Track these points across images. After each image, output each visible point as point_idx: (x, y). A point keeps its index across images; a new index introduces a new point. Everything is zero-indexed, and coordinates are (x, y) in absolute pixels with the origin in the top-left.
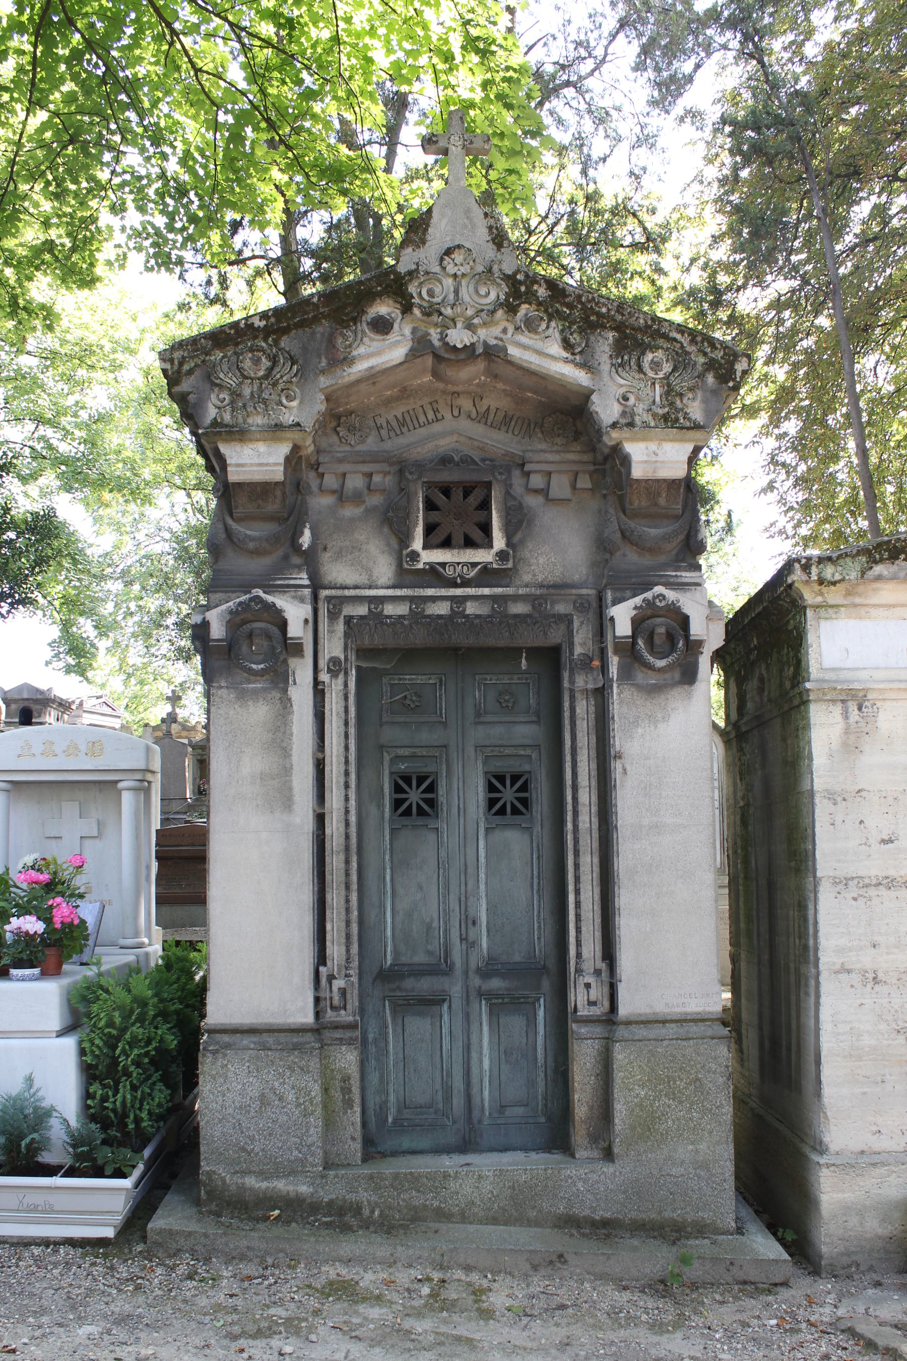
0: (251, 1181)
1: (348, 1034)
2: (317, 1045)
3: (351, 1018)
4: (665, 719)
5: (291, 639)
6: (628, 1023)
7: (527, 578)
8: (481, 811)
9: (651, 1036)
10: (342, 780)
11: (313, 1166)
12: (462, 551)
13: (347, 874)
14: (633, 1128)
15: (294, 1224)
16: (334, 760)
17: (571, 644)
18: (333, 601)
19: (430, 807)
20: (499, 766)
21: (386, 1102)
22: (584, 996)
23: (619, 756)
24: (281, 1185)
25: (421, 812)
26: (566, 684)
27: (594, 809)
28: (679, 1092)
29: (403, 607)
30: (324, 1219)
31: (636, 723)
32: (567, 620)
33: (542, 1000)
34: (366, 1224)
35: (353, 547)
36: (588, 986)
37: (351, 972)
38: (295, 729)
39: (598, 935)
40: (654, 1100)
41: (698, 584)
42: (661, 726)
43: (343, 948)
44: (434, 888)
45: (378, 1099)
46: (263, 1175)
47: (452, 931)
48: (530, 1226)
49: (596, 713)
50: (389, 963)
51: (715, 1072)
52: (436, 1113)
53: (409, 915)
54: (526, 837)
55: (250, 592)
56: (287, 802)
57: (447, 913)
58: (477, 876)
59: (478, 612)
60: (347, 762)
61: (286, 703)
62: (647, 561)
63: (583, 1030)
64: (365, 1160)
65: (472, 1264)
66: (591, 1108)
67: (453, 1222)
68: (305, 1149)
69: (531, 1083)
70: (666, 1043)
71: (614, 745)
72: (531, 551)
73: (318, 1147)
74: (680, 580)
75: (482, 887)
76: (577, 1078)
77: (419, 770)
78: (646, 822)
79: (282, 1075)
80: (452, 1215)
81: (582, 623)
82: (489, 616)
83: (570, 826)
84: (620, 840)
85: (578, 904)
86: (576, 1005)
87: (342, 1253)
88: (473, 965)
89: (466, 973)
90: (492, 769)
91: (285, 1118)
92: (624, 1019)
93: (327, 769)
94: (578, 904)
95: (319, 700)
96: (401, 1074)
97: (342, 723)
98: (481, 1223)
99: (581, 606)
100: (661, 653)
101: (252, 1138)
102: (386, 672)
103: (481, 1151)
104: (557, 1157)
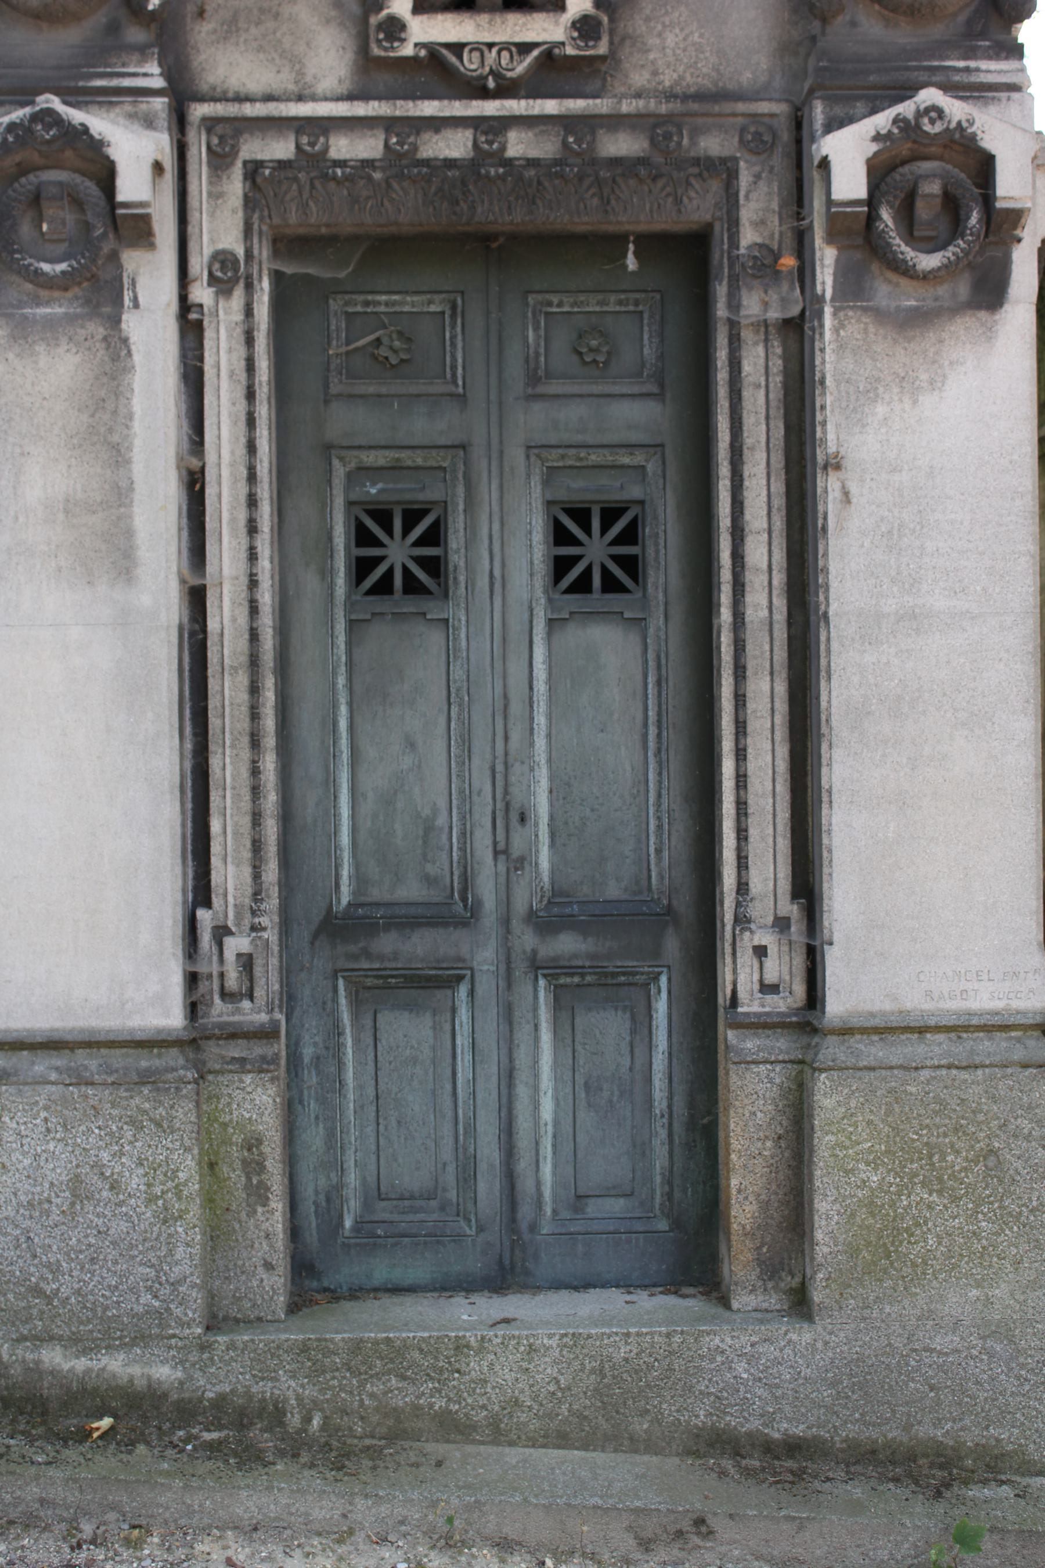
0: (53, 1357)
1: (258, 1049)
2: (190, 1075)
3: (263, 1017)
4: (935, 384)
5: (125, 205)
6: (846, 1031)
7: (639, 79)
8: (539, 583)
9: (894, 1061)
10: (242, 516)
11: (182, 1324)
12: (498, 18)
13: (255, 715)
14: (853, 1252)
15: (141, 1449)
16: (225, 472)
17: (734, 223)
18: (219, 129)
19: (429, 577)
20: (577, 488)
21: (340, 1187)
22: (753, 972)
23: (835, 464)
24: (118, 1366)
25: (412, 586)
26: (721, 311)
27: (779, 579)
28: (953, 1177)
29: (372, 142)
30: (207, 1436)
31: (871, 393)
32: (724, 170)
33: (664, 980)
34: (294, 1447)
35: (262, 11)
36: (761, 952)
37: (265, 921)
38: (138, 405)
39: (784, 844)
40: (899, 1194)
41: (1015, 88)
42: (927, 400)
43: (247, 871)
44: (440, 745)
45: (322, 1182)
46: (79, 1344)
47: (478, 833)
48: (636, 1451)
49: (786, 372)
50: (345, 901)
51: (1028, 1138)
52: (442, 1208)
53: (387, 801)
54: (634, 639)
55: (32, 103)
56: (121, 559)
57: (467, 797)
58: (526, 720)
59: (533, 153)
60: (252, 477)
61: (118, 348)
62: (903, 35)
63: (751, 1044)
64: (293, 1308)
65: (513, 1536)
66: (765, 1206)
67: (474, 1442)
68: (165, 1291)
69: (640, 1149)
70: (925, 1074)
71: (824, 441)
72: (648, 20)
73: (194, 1285)
74: (974, 78)
75: (540, 742)
76: (735, 1144)
77: (408, 497)
78: (890, 605)
79: (116, 1138)
80: (474, 1427)
81: (758, 177)
82: (556, 162)
83: (725, 615)
84: (835, 645)
85: (741, 780)
86: (734, 992)
87: (240, 1511)
88: (521, 904)
89: (506, 922)
90: (562, 495)
91: (124, 1226)
92: (837, 1023)
93: (210, 492)
94: (741, 780)
95: (191, 344)
96: (370, 1130)
97: (240, 392)
98: (533, 1443)
99: (757, 139)
100: (930, 239)
101: (55, 1269)
102: (335, 288)
103: (535, 1288)
104: (693, 1305)
